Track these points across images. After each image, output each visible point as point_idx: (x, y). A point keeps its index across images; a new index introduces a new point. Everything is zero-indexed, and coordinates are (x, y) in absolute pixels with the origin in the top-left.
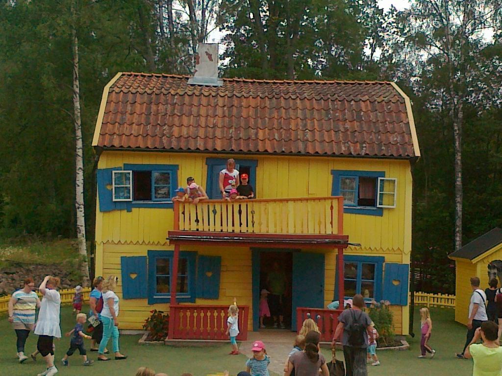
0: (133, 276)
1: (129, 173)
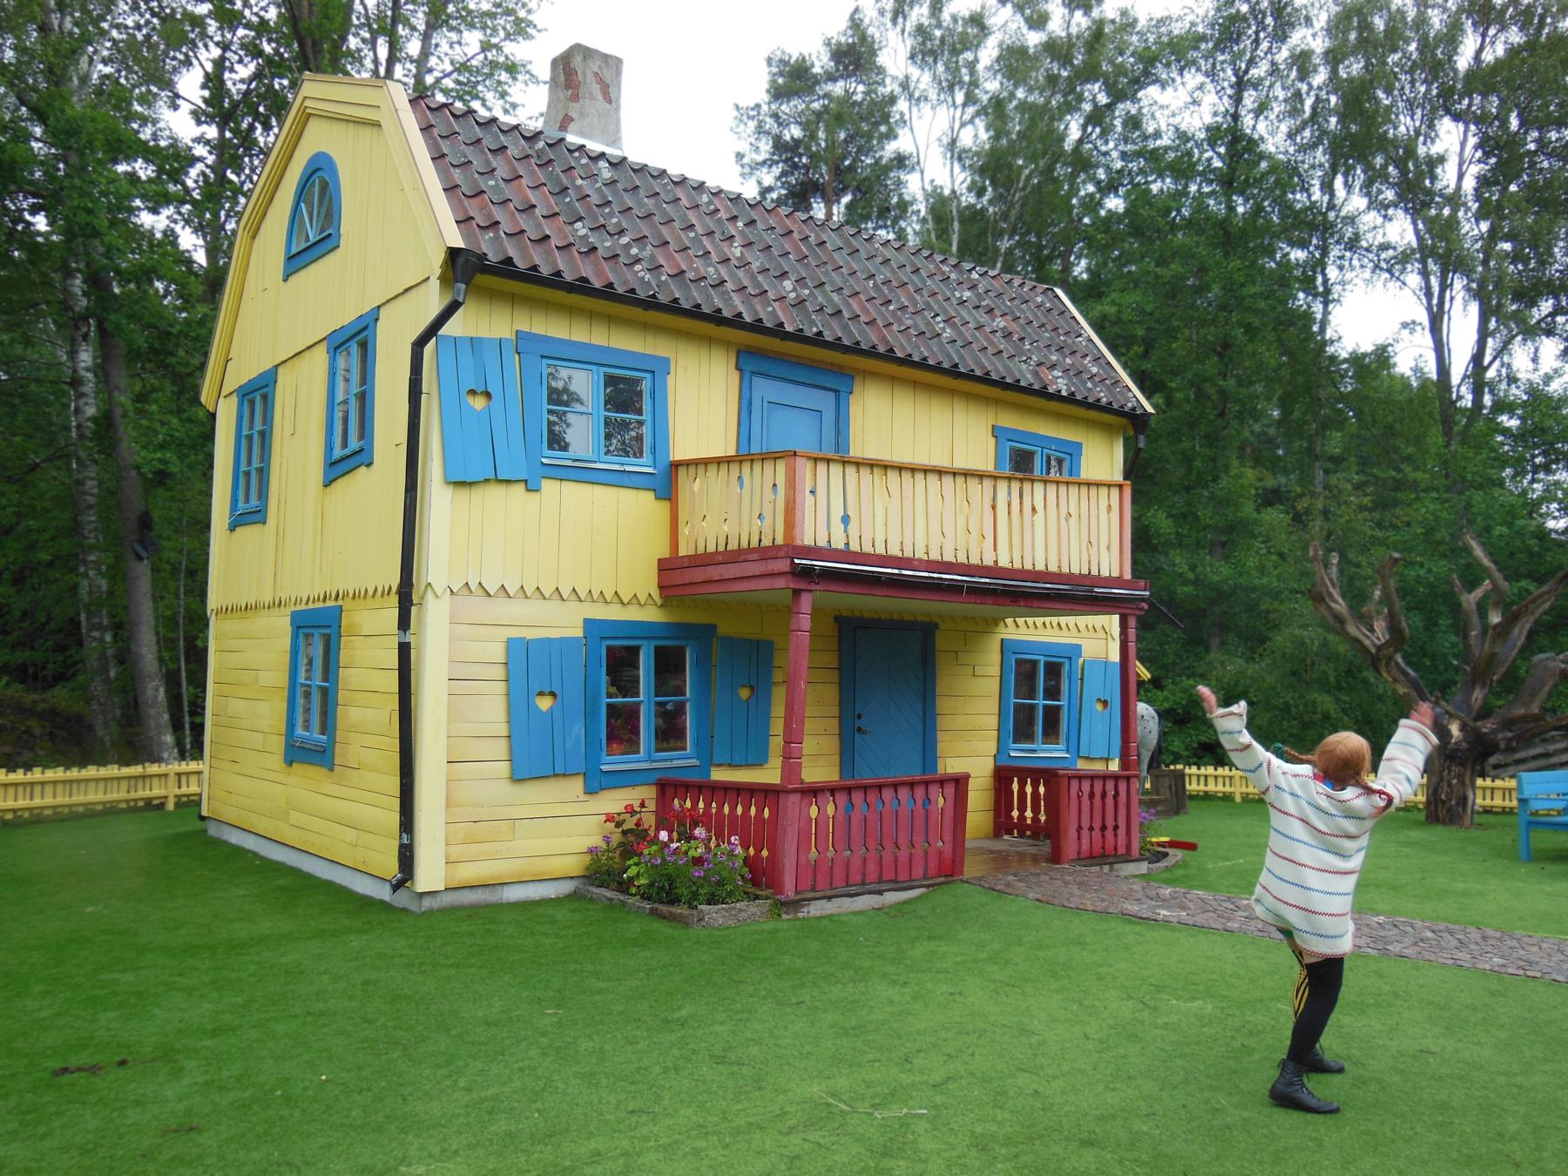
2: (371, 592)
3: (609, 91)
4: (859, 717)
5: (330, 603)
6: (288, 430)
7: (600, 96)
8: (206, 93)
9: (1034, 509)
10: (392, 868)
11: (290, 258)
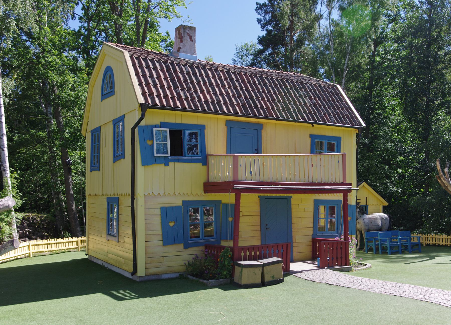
0: (172, 224)
1: (166, 131)
2: (125, 195)
3: (192, 39)
4: (267, 225)
5: (116, 196)
6: (104, 146)
7: (189, 40)
8: (83, 12)
9: (312, 165)
10: (131, 270)
11: (102, 95)
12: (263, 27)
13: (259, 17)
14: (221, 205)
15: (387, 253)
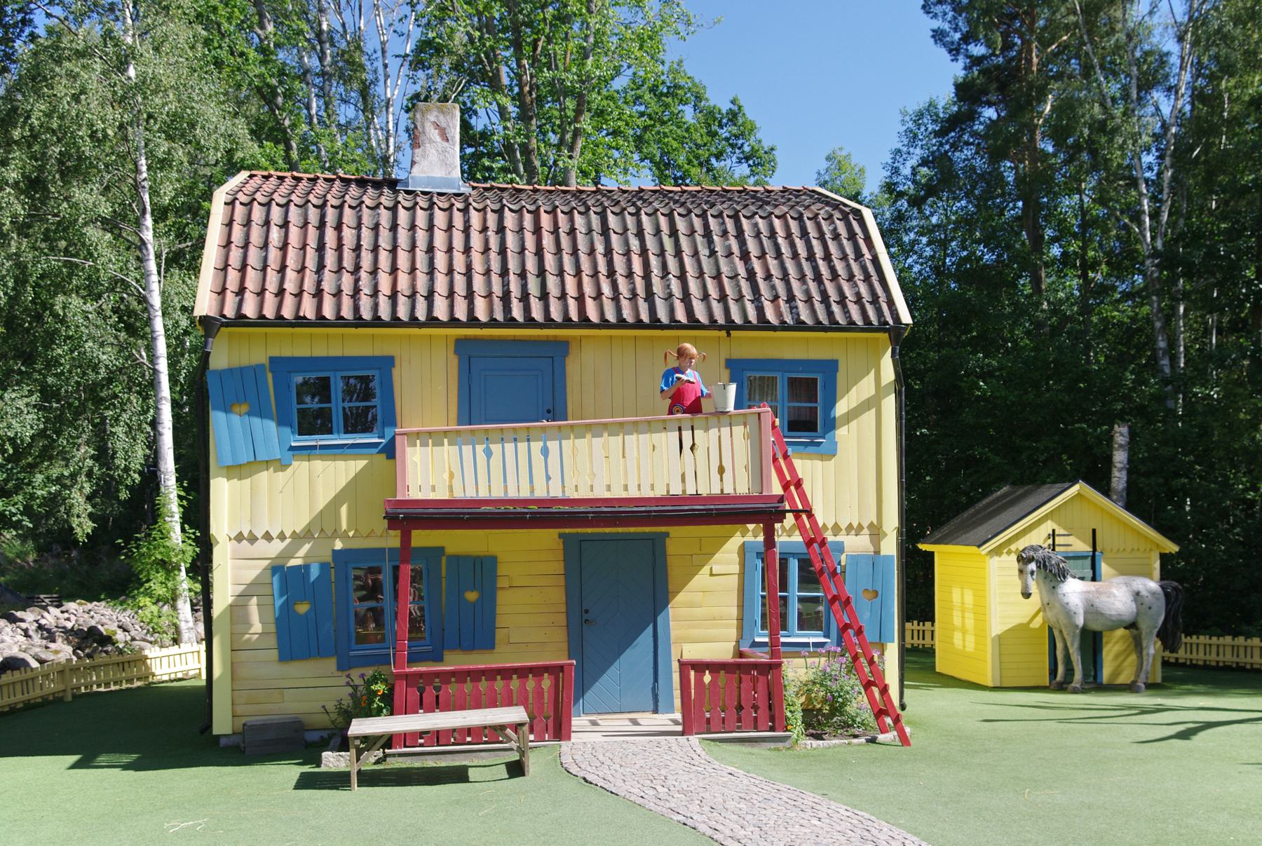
4: (587, 611)
12: (954, 51)
13: (936, 24)
14: (444, 559)
15: (1139, 687)
